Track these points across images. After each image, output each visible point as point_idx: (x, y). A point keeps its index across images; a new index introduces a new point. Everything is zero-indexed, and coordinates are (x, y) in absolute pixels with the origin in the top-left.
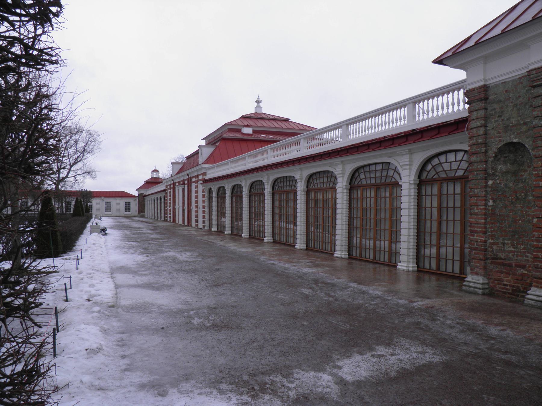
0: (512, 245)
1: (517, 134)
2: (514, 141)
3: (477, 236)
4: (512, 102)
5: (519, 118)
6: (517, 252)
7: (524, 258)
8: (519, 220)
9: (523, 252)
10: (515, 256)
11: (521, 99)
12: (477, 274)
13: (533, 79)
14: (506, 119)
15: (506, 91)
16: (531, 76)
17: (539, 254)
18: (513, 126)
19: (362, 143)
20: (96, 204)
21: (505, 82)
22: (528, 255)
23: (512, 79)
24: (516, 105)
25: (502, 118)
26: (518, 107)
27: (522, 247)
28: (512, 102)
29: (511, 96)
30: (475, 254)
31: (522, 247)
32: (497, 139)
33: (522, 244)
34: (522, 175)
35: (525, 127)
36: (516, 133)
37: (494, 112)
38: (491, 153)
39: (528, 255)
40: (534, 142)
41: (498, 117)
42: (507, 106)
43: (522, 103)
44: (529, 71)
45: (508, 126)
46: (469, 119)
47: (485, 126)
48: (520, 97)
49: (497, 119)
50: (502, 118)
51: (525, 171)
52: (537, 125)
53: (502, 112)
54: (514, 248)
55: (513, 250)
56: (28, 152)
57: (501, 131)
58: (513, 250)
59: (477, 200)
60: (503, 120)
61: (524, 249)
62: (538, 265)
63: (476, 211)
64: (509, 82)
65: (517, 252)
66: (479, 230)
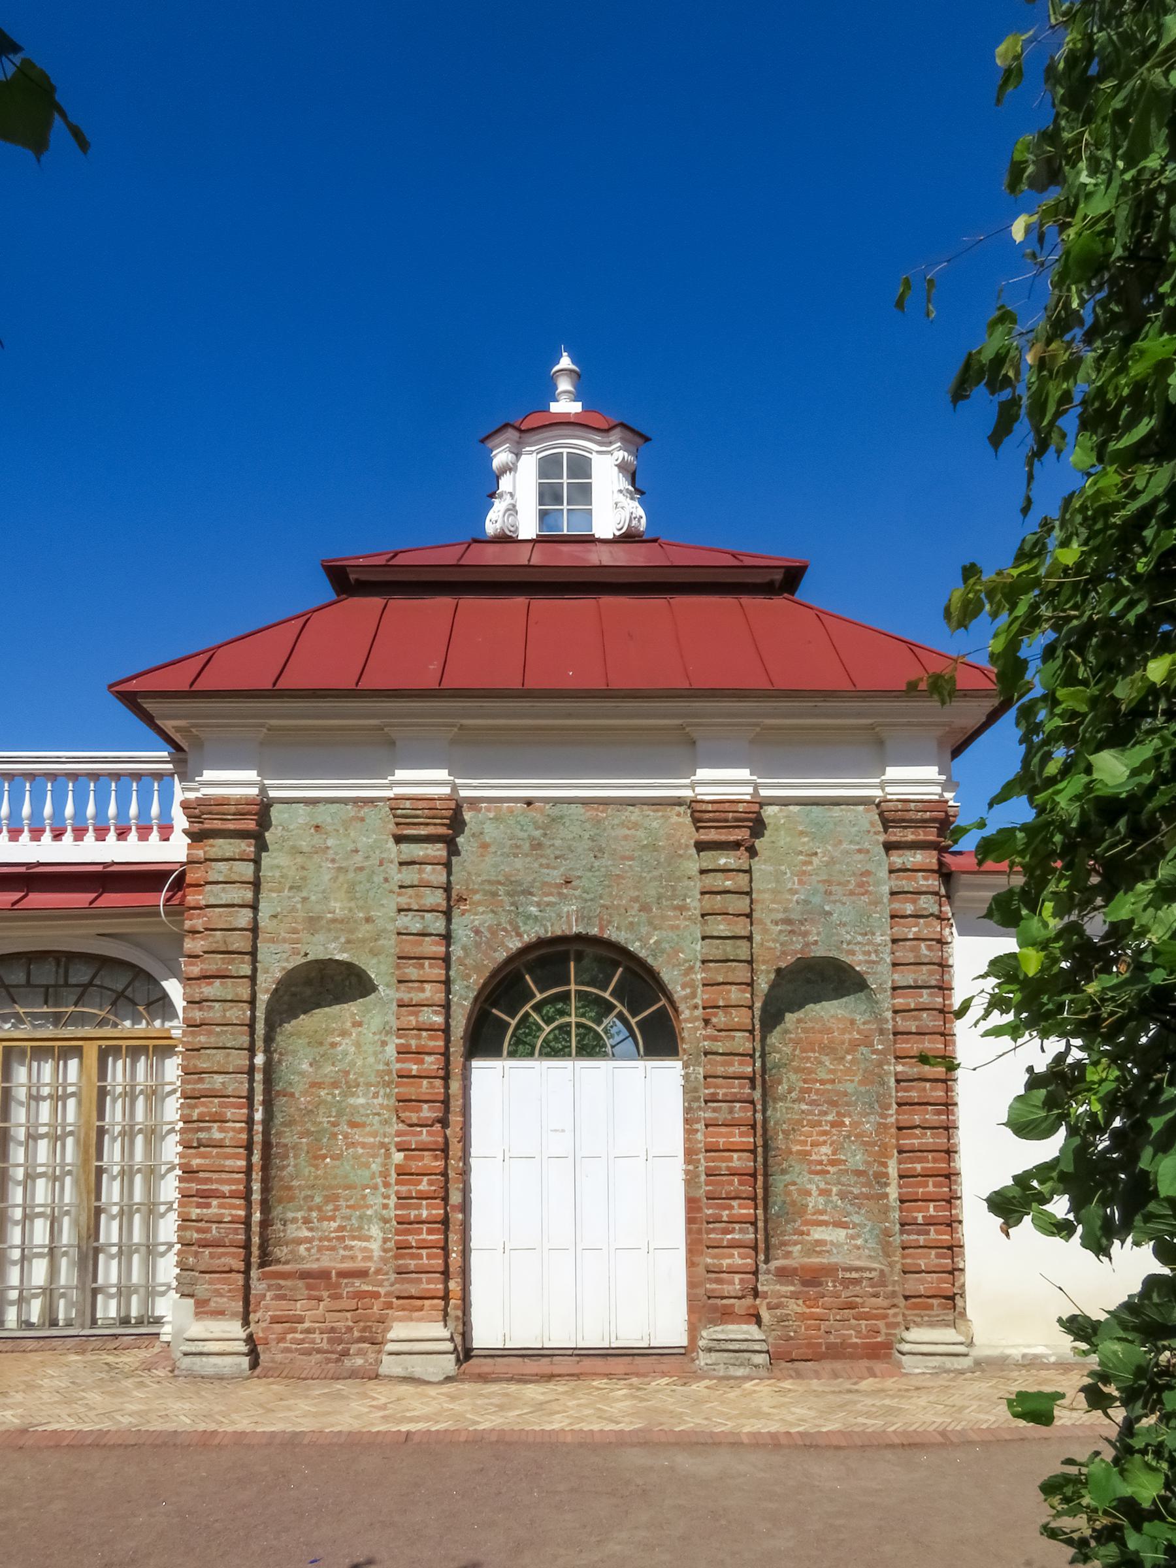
0: (307, 1221)
1: (348, 942)
2: (337, 957)
3: (220, 1206)
4: (333, 861)
5: (352, 904)
6: (321, 1240)
7: (342, 1252)
8: (324, 1157)
9: (338, 1238)
10: (313, 1251)
12: (219, 1313)
17: (410, 1238)
18: (334, 921)
22: (353, 1243)
25: (304, 894)
27: (334, 1225)
30: (212, 1256)
31: (334, 1225)
32: (287, 946)
33: (333, 1219)
34: (334, 1045)
35: (368, 927)
36: (343, 940)
38: (267, 983)
39: (353, 1243)
40: (398, 967)
41: (291, 888)
45: (319, 918)
47: (255, 907)
48: (357, 851)
51: (344, 1033)
52: (407, 928)
54: (311, 1229)
55: (309, 1234)
56: (1126, 384)
57: (300, 927)
58: (309, 1234)
59: (221, 1105)
61: (341, 1228)
62: (406, 1265)
63: (217, 1135)
65: (321, 1240)
66: (226, 1189)
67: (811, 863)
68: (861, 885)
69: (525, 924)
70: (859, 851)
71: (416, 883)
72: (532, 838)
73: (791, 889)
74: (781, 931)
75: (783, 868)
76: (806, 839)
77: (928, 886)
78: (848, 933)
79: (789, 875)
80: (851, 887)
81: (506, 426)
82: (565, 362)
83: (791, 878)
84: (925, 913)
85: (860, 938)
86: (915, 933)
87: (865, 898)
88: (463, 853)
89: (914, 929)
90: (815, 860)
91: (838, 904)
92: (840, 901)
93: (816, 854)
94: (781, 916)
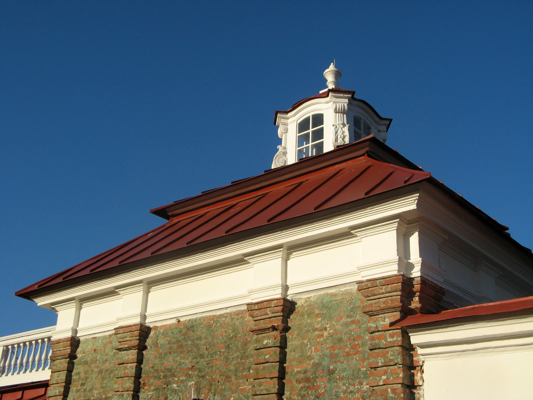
11: (107, 364)
13: (121, 340)
14: (88, 389)
15: (95, 350)
16: (118, 335)
19: (32, 383)
20: (167, 210)
21: (95, 338)
23: (234, 310)
24: (101, 372)
26: (103, 374)
28: (98, 367)
29: (98, 357)
37: (78, 377)
42: (92, 371)
43: (107, 370)
44: (117, 328)
46: (50, 383)
48: (106, 360)
49: (79, 388)
50: (85, 387)
53: (86, 378)
60: (85, 390)
64: (99, 338)
67: (322, 336)
68: (354, 347)
69: (171, 395)
70: (353, 322)
71: (122, 376)
72: (178, 341)
73: (309, 356)
74: (302, 388)
75: (306, 341)
76: (320, 319)
77: (394, 342)
78: (344, 384)
79: (309, 346)
80: (347, 350)
81: (277, 113)
82: (332, 67)
83: (310, 348)
84: (392, 363)
85: (352, 388)
86: (384, 380)
87: (357, 357)
88: (297, 302)
89: (384, 377)
90: (326, 334)
91: (339, 364)
92: (339, 361)
93: (325, 329)
94: (302, 376)
